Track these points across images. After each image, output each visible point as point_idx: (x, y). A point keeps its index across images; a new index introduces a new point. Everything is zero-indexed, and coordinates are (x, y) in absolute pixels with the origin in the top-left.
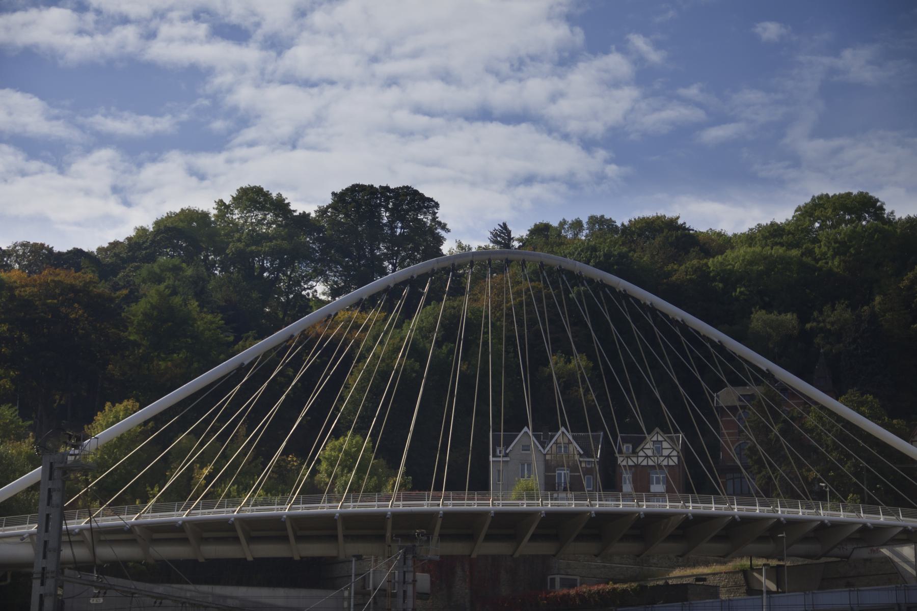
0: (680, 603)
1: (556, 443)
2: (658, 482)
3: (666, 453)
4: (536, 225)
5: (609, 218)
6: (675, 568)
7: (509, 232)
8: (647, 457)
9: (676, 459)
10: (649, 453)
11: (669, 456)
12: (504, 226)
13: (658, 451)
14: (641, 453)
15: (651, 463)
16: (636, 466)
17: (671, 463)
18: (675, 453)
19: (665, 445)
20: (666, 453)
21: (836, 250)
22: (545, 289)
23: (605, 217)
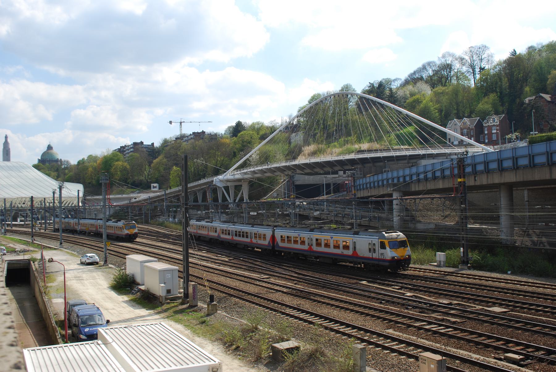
0: (545, 143)
1: (463, 122)
2: (494, 130)
3: (496, 121)
4: (313, 98)
5: (201, 131)
6: (229, 242)
7: (515, 52)
8: (491, 123)
9: (499, 123)
10: (492, 122)
11: (497, 122)
12: (514, 50)
13: (494, 121)
14: (489, 122)
15: (492, 125)
16: (488, 126)
17: (497, 124)
18: (498, 121)
19: (496, 119)
20: (496, 121)
21: (524, 77)
22: (166, 157)
23: (144, 144)
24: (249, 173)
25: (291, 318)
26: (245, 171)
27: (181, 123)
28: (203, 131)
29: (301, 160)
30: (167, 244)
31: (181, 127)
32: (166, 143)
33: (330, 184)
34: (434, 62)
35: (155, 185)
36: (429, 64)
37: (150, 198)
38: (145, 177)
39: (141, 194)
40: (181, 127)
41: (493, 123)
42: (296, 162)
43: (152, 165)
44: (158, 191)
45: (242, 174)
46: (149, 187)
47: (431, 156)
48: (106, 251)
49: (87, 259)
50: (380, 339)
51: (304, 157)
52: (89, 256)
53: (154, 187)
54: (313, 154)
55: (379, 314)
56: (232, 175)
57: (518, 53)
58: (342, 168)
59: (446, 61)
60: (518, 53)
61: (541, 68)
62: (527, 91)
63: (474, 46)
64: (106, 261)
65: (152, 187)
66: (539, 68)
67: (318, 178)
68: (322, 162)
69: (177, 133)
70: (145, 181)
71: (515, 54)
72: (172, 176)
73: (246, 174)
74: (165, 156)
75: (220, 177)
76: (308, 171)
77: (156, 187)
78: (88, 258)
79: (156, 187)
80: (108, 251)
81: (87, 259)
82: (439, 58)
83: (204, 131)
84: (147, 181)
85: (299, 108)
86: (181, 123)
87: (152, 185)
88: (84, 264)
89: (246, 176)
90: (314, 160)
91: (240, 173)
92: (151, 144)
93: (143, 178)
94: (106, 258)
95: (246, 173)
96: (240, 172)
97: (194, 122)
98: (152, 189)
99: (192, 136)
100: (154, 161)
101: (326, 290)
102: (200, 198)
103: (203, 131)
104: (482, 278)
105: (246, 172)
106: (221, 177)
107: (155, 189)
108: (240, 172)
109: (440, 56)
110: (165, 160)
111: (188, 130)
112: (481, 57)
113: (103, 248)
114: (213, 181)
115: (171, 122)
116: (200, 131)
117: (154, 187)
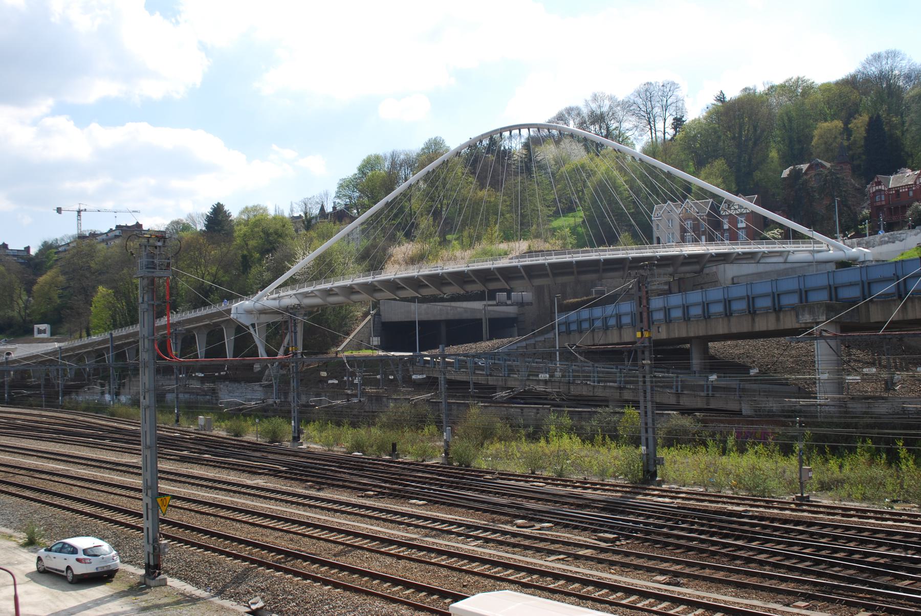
5: (134, 223)
8: (735, 209)
12: (721, 92)
14: (732, 208)
22: (64, 273)
23: (10, 247)
24: (317, 293)
25: (192, 547)
26: (328, 286)
27: (79, 212)
28: (137, 223)
29: (391, 272)
30: (211, 468)
31: (79, 219)
32: (47, 248)
33: (481, 319)
34: (578, 108)
35: (43, 327)
36: (569, 111)
37: (578, 302)
38: (19, 312)
39: (17, 345)
40: (79, 219)
41: (739, 210)
42: (383, 276)
43: (35, 288)
44: (50, 339)
45: (299, 296)
46: (30, 332)
47: (695, 260)
48: (156, 529)
49: (78, 560)
50: (374, 582)
51: (397, 266)
52: (85, 551)
53: (40, 332)
54: (413, 260)
55: (297, 529)
56: (274, 299)
57: (728, 99)
58: (440, 290)
59: (600, 107)
60: (728, 99)
61: (790, 120)
62: (772, 158)
63: (653, 82)
64: (153, 569)
65: (36, 330)
66: (786, 118)
67: (438, 307)
68: (446, 273)
69: (73, 231)
70: (19, 318)
71: (724, 98)
72: (95, 307)
73: (306, 297)
74: (61, 272)
75: (247, 303)
76: (410, 293)
77: (44, 332)
78: (81, 556)
79: (44, 332)
80: (165, 528)
81: (78, 560)
82: (586, 101)
83: (140, 223)
84: (24, 320)
85: (340, 180)
86: (79, 212)
87: (36, 326)
88: (64, 578)
89: (307, 301)
90: (413, 272)
91: (295, 295)
92: (23, 249)
93: (15, 314)
94: (157, 551)
95: (306, 295)
96: (294, 292)
97: (106, 211)
98: (37, 336)
99: (117, 233)
100: (41, 279)
101: (346, 517)
102: (201, 348)
103: (137, 223)
104: (836, 511)
105: (312, 292)
106: (247, 302)
107: (42, 336)
108: (294, 292)
109: (589, 98)
110: (61, 278)
111: (103, 225)
112: (665, 101)
113: (141, 516)
114: (229, 311)
115: (59, 210)
116: (131, 223)
117: (40, 332)
